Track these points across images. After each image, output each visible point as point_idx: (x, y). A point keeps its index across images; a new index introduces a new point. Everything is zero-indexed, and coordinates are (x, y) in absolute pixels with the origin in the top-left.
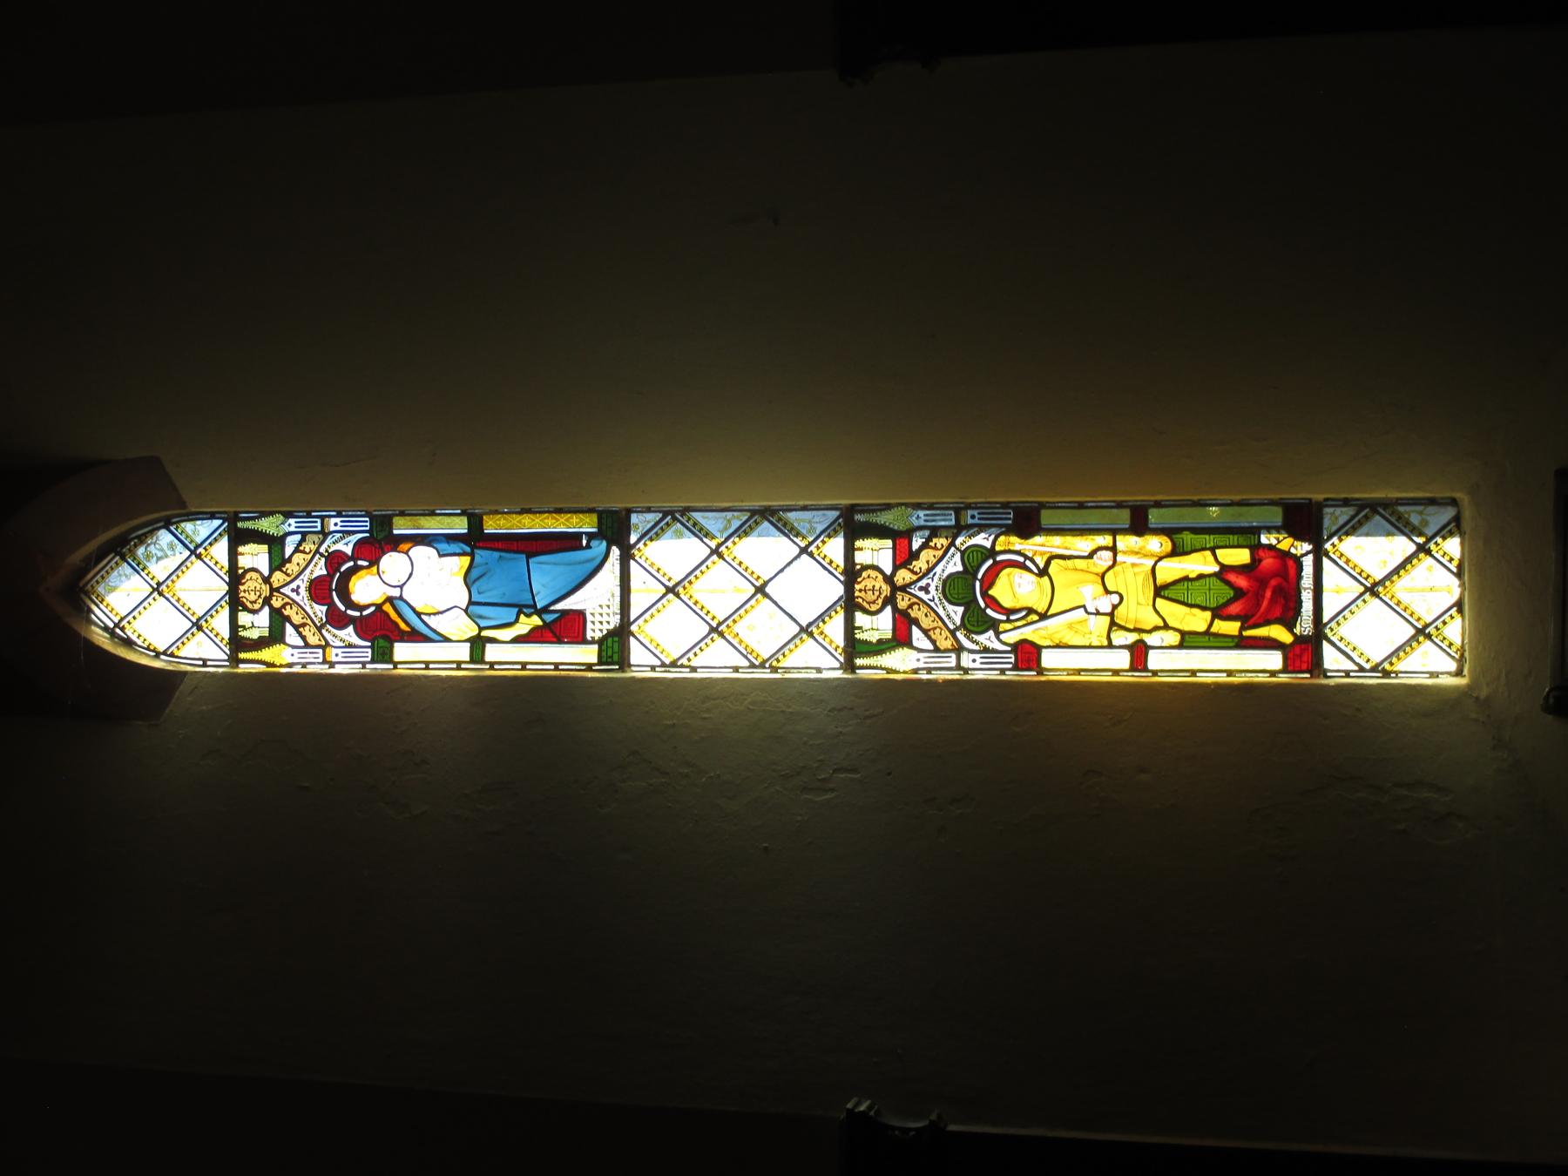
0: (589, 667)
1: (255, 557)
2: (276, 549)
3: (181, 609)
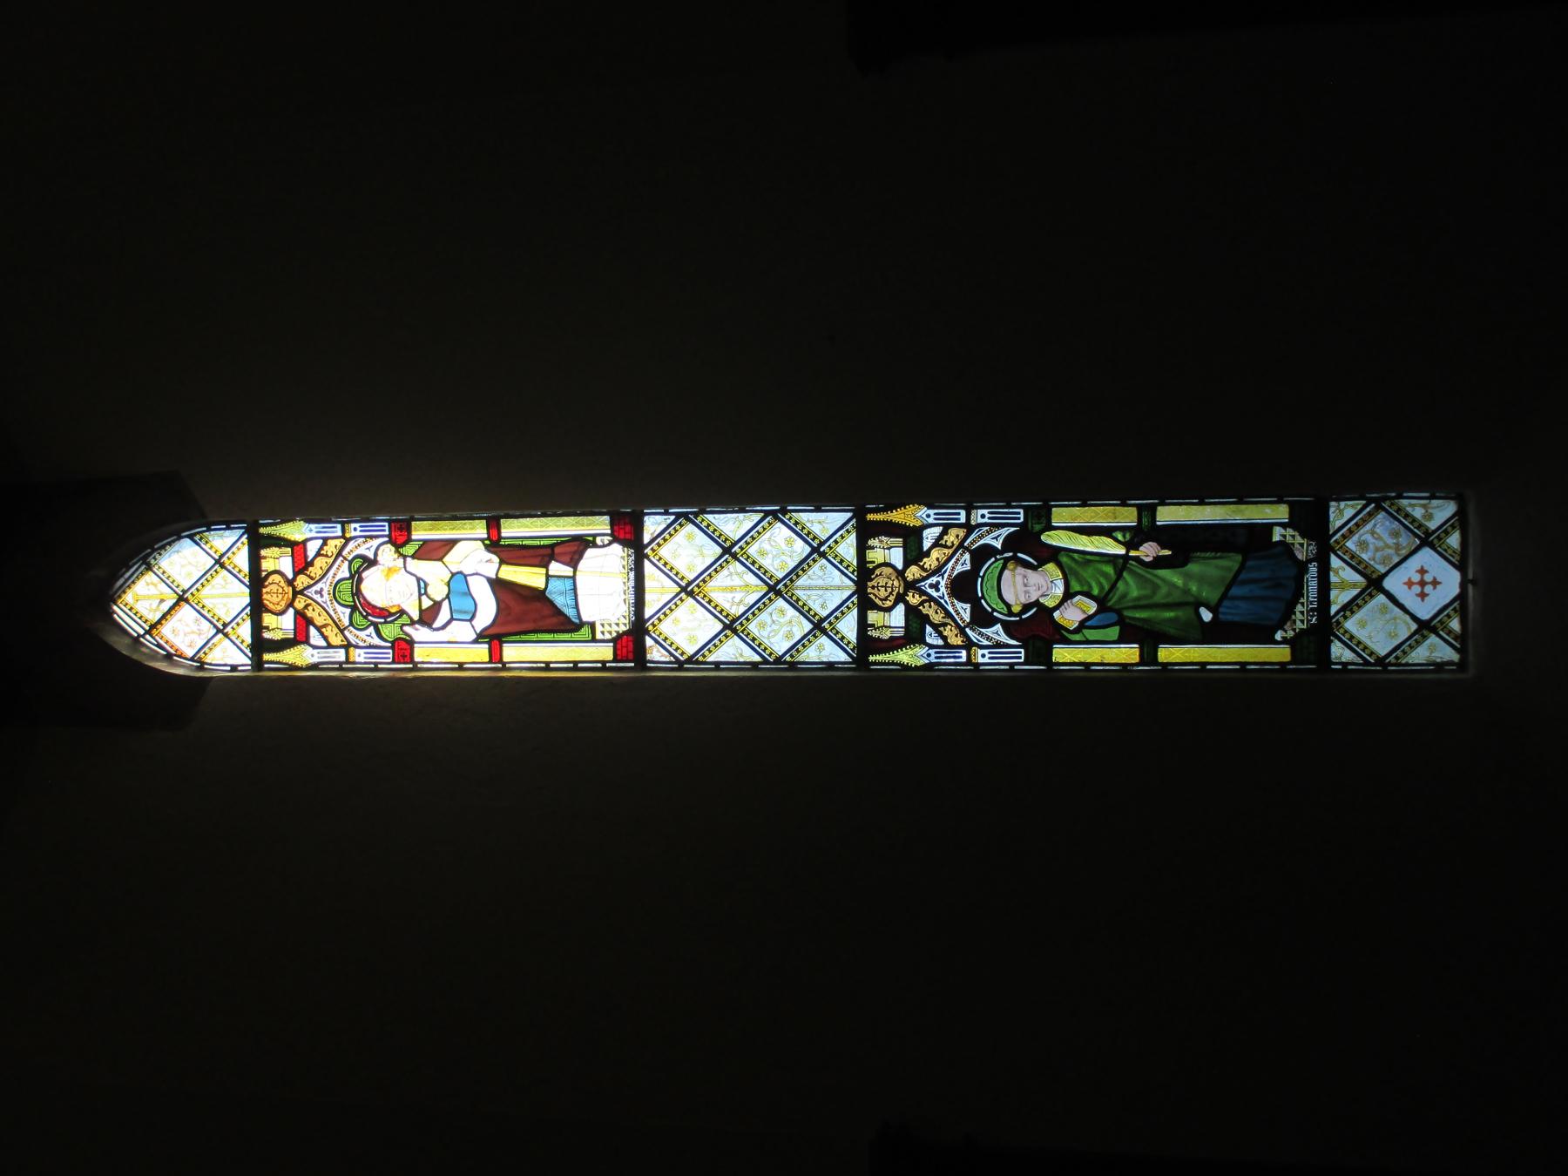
1: (888, 552)
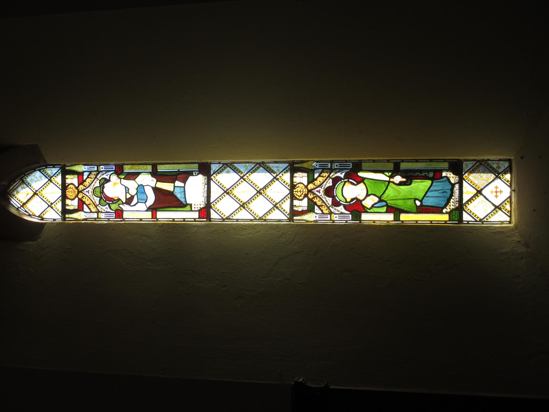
0: (446, 222)
1: (72, 180)
2: (80, 177)
3: (270, 200)
